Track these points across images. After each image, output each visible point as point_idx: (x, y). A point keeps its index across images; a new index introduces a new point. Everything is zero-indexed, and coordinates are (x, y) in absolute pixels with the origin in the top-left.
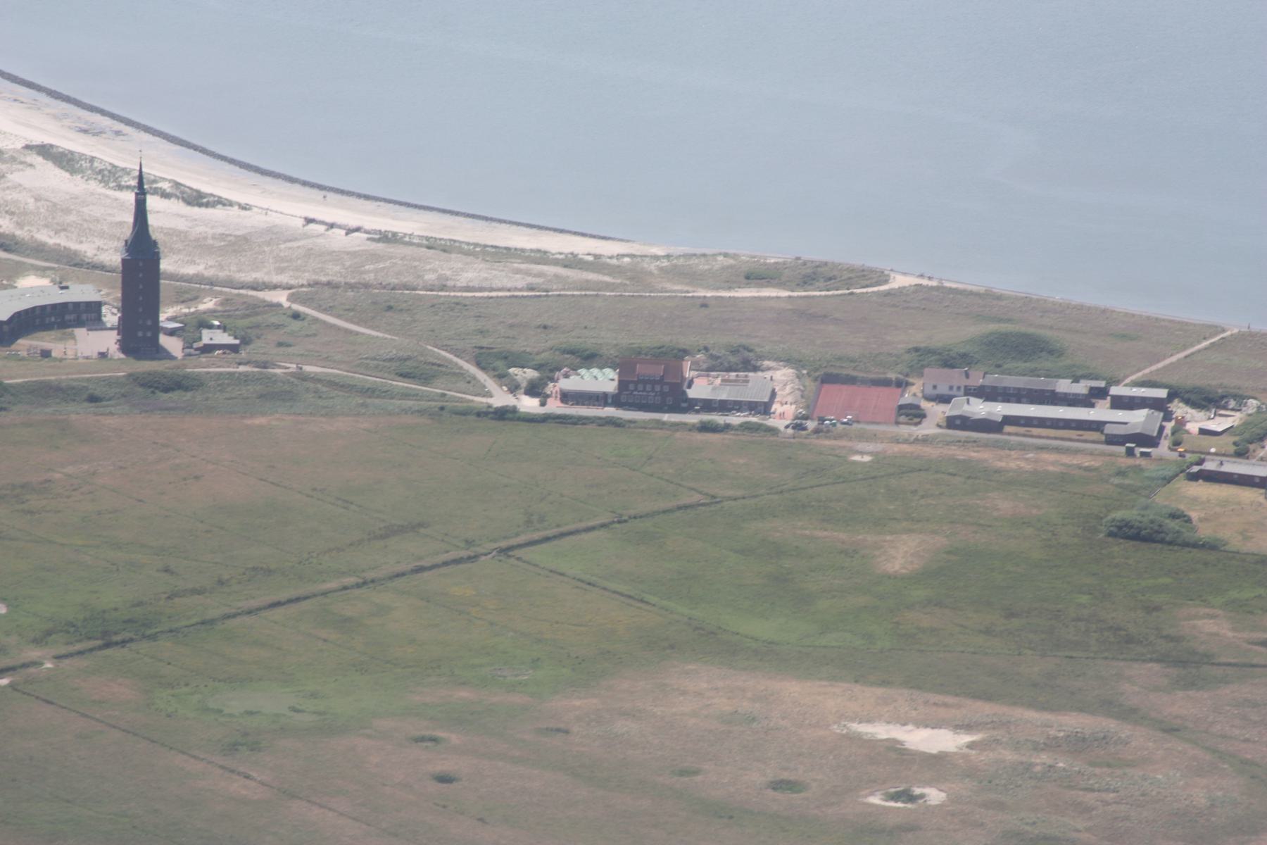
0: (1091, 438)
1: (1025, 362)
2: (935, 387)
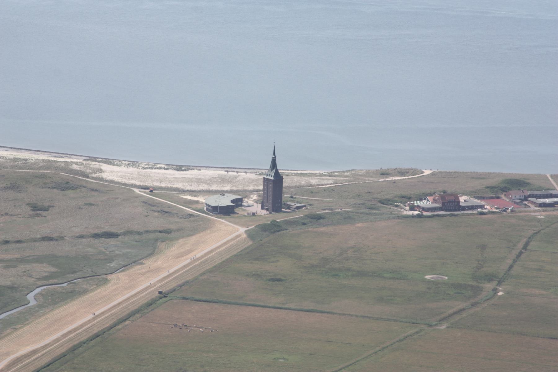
1: (82, 235)
2: (515, 197)
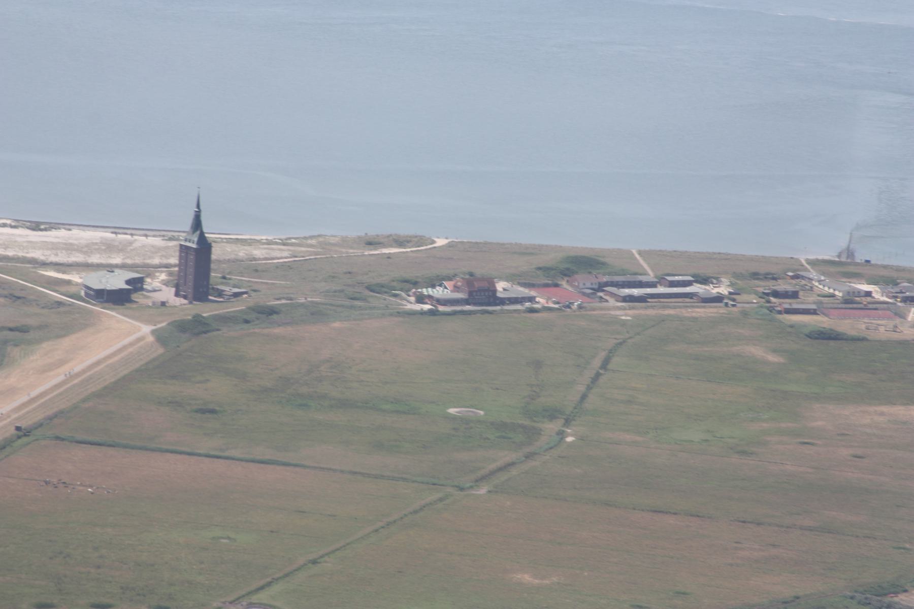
0: (687, 301)
